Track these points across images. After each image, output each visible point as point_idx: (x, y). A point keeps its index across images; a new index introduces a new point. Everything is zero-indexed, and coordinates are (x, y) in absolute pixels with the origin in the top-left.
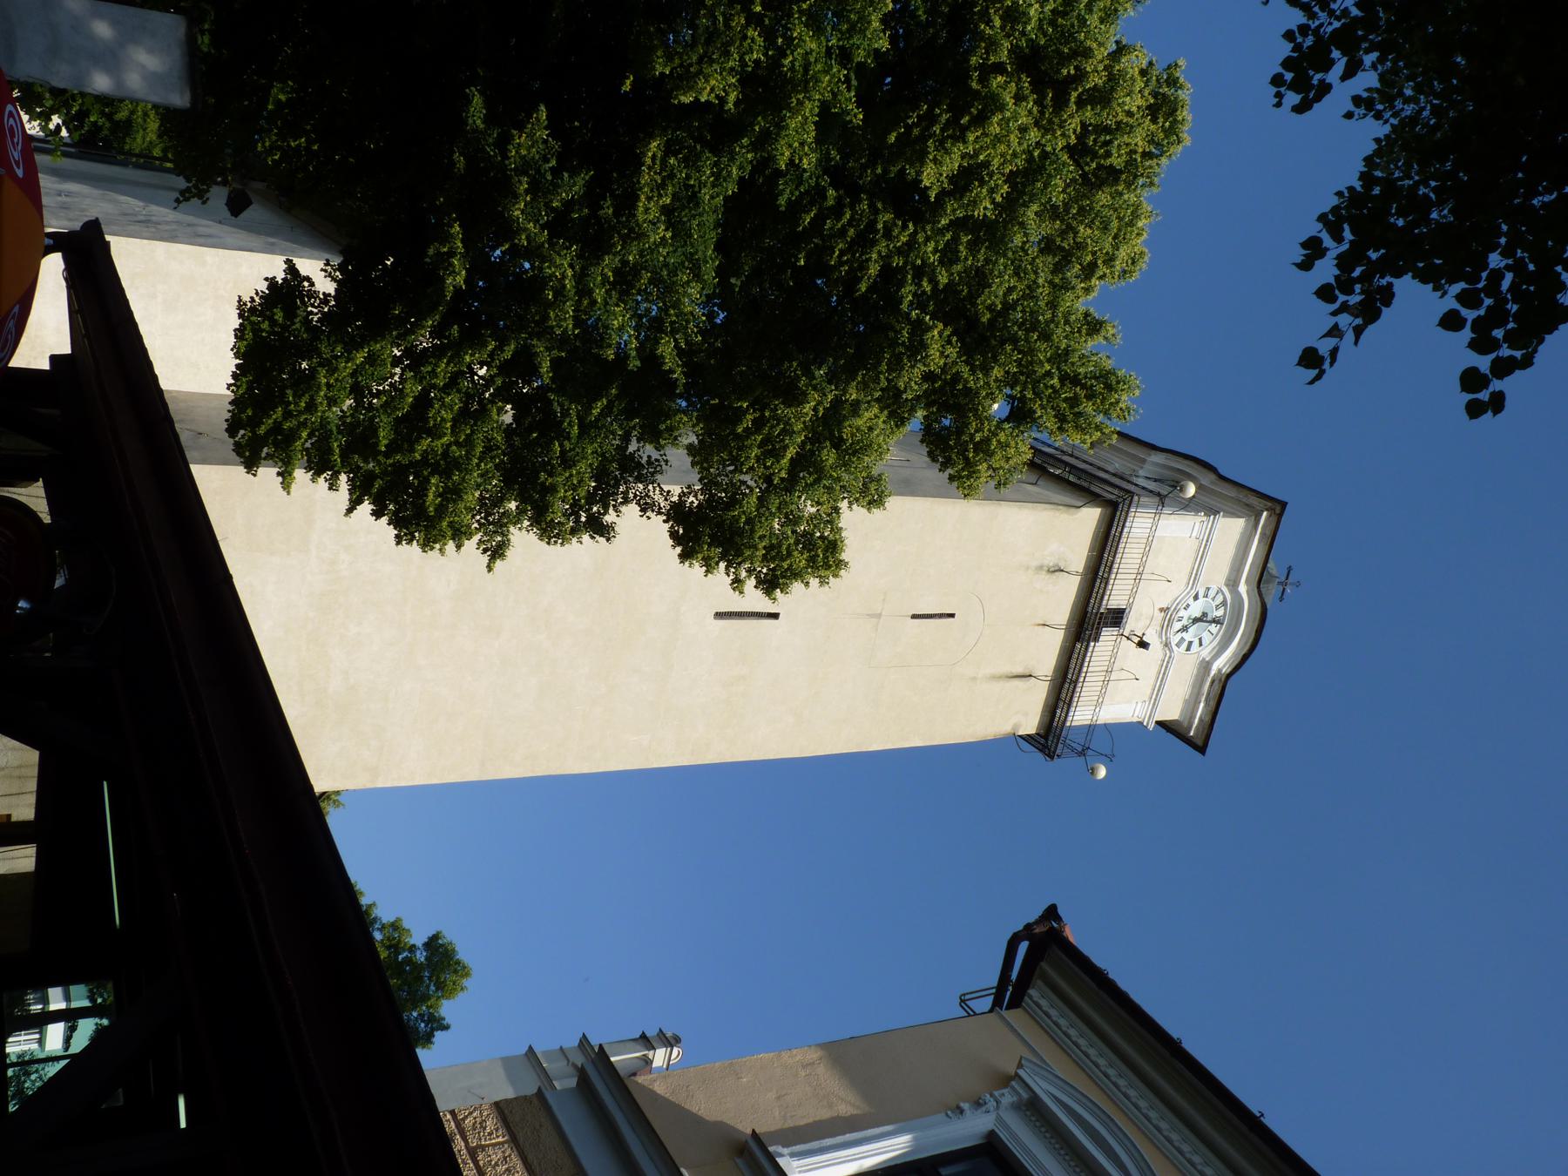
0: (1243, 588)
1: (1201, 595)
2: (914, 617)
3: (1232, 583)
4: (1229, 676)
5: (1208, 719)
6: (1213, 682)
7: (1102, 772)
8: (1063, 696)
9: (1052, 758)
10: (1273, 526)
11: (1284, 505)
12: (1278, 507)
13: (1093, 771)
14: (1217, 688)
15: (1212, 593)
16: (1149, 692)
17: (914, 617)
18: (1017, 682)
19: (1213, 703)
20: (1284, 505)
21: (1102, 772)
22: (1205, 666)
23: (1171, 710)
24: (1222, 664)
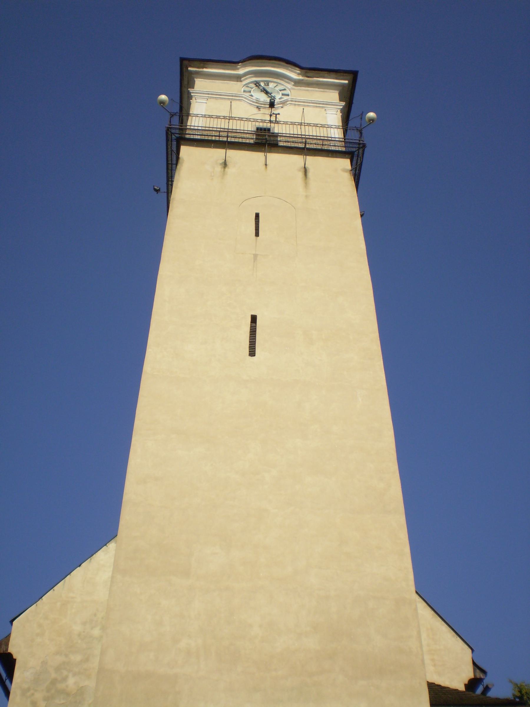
0: (241, 71)
1: (250, 94)
2: (257, 234)
3: (238, 78)
4: (301, 68)
5: (333, 75)
6: (308, 77)
7: (372, 115)
8: (319, 147)
9: (364, 146)
10: (196, 63)
11: (182, 60)
12: (185, 62)
13: (372, 120)
14: (311, 73)
15: (247, 89)
16: (318, 109)
17: (257, 234)
18: (310, 174)
19: (322, 73)
20: (182, 60)
21: (372, 115)
22: (297, 83)
23: (333, 96)
24: (294, 74)
